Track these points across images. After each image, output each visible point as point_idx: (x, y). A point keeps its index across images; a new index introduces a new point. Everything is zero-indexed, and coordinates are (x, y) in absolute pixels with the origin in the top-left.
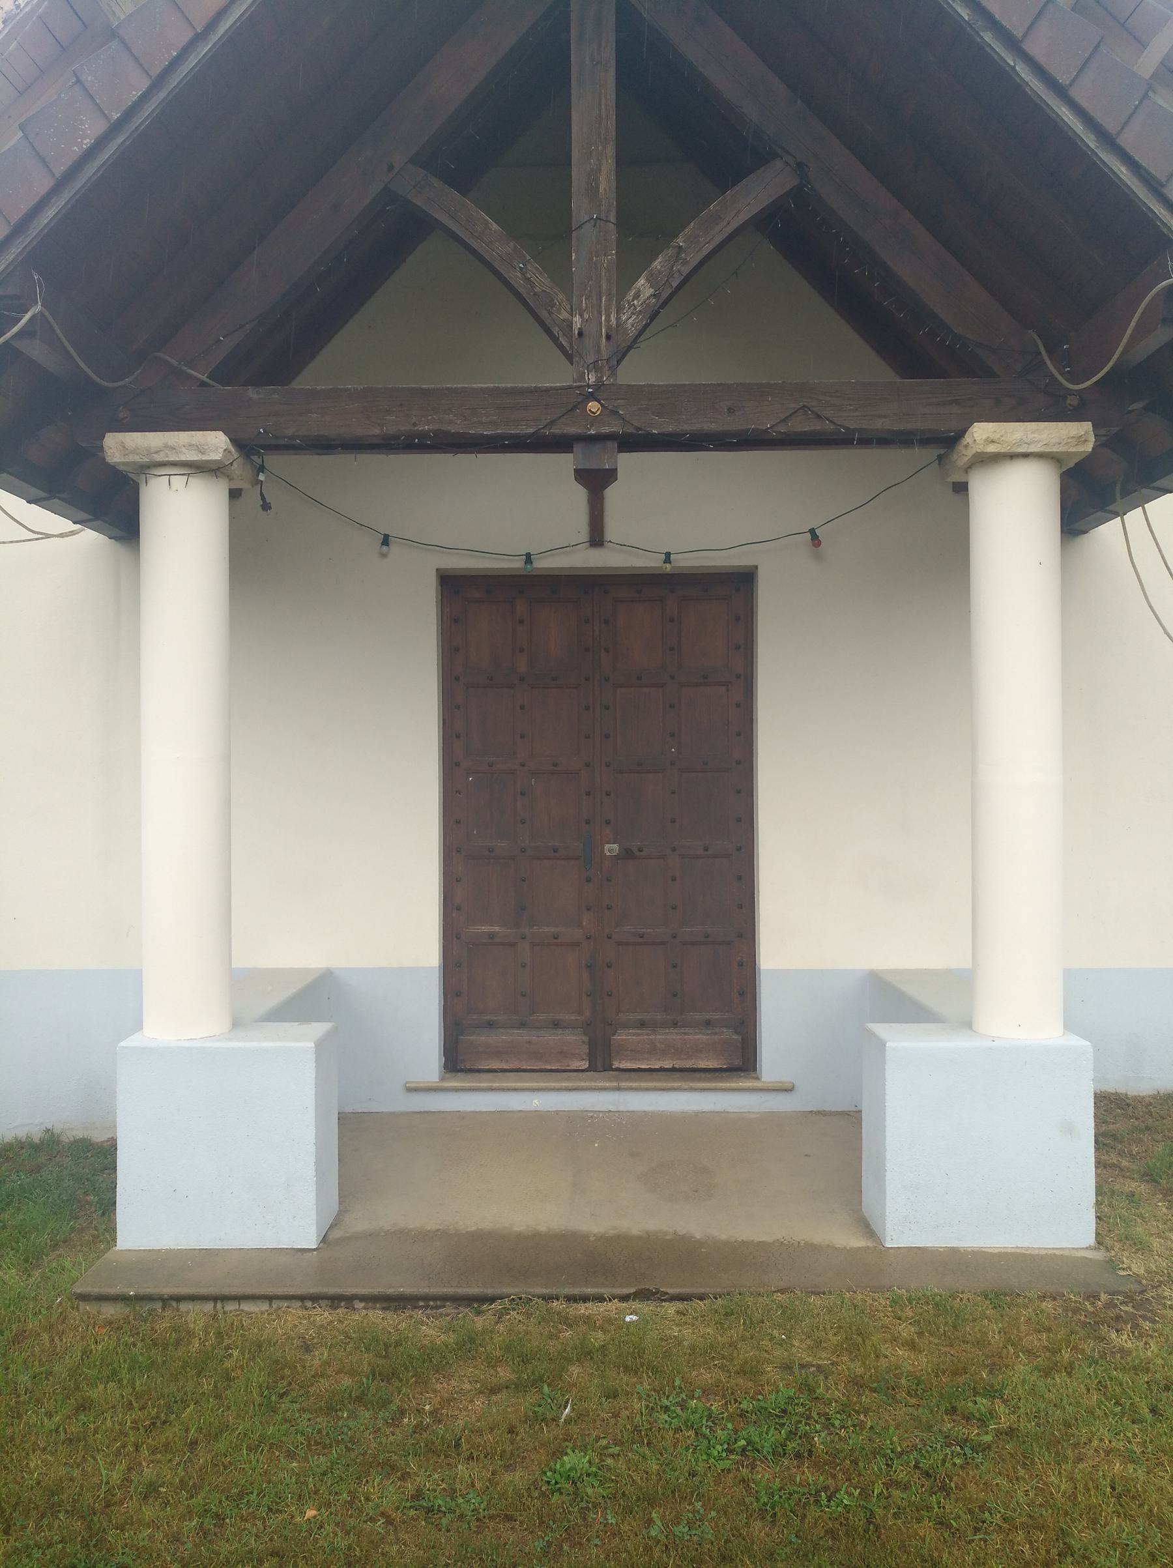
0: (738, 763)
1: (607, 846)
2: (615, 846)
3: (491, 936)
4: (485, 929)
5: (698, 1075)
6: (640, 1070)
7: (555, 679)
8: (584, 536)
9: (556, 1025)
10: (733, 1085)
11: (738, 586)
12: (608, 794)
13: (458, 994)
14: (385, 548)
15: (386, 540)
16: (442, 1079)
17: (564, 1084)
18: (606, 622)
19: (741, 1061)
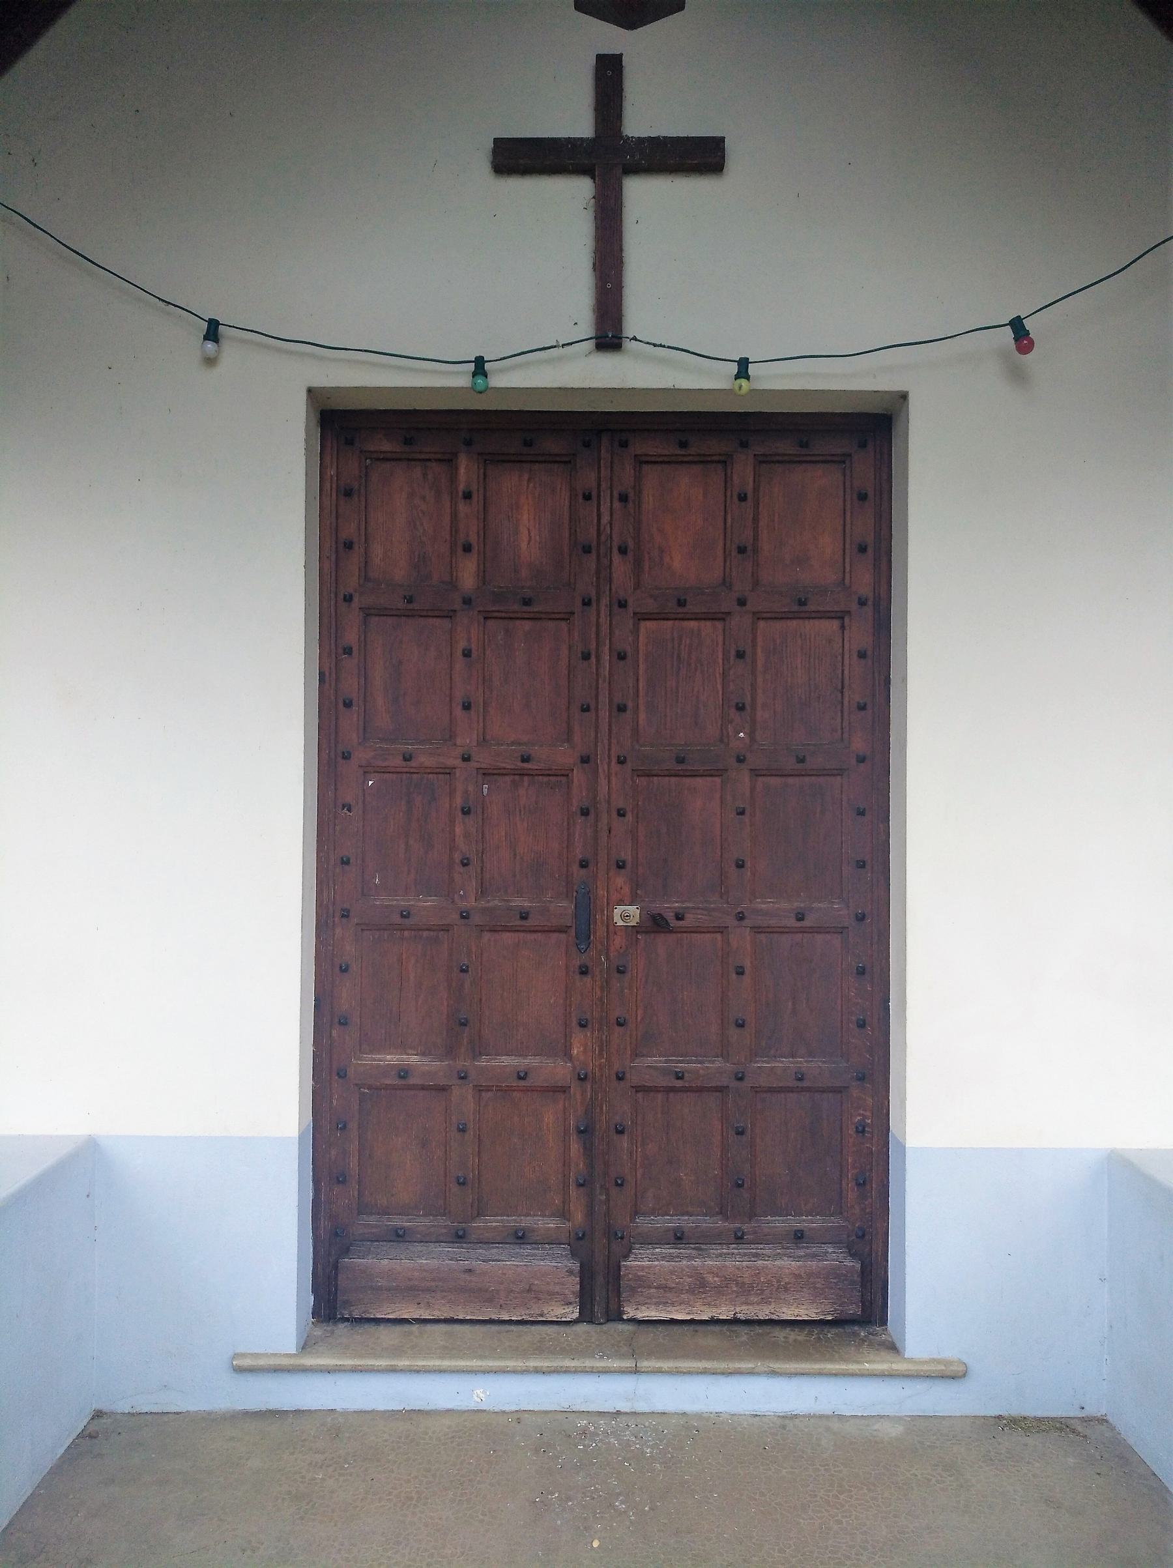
0: (861, 760)
1: (618, 910)
2: (633, 911)
3: (404, 1073)
4: (391, 1059)
5: (780, 1334)
6: (673, 1322)
7: (527, 602)
8: (584, 324)
9: (520, 1237)
10: (853, 1367)
11: (860, 440)
12: (621, 813)
13: (341, 1179)
14: (210, 345)
15: (213, 331)
16: (306, 1346)
17: (532, 1363)
18: (624, 498)
19: (861, 1311)
